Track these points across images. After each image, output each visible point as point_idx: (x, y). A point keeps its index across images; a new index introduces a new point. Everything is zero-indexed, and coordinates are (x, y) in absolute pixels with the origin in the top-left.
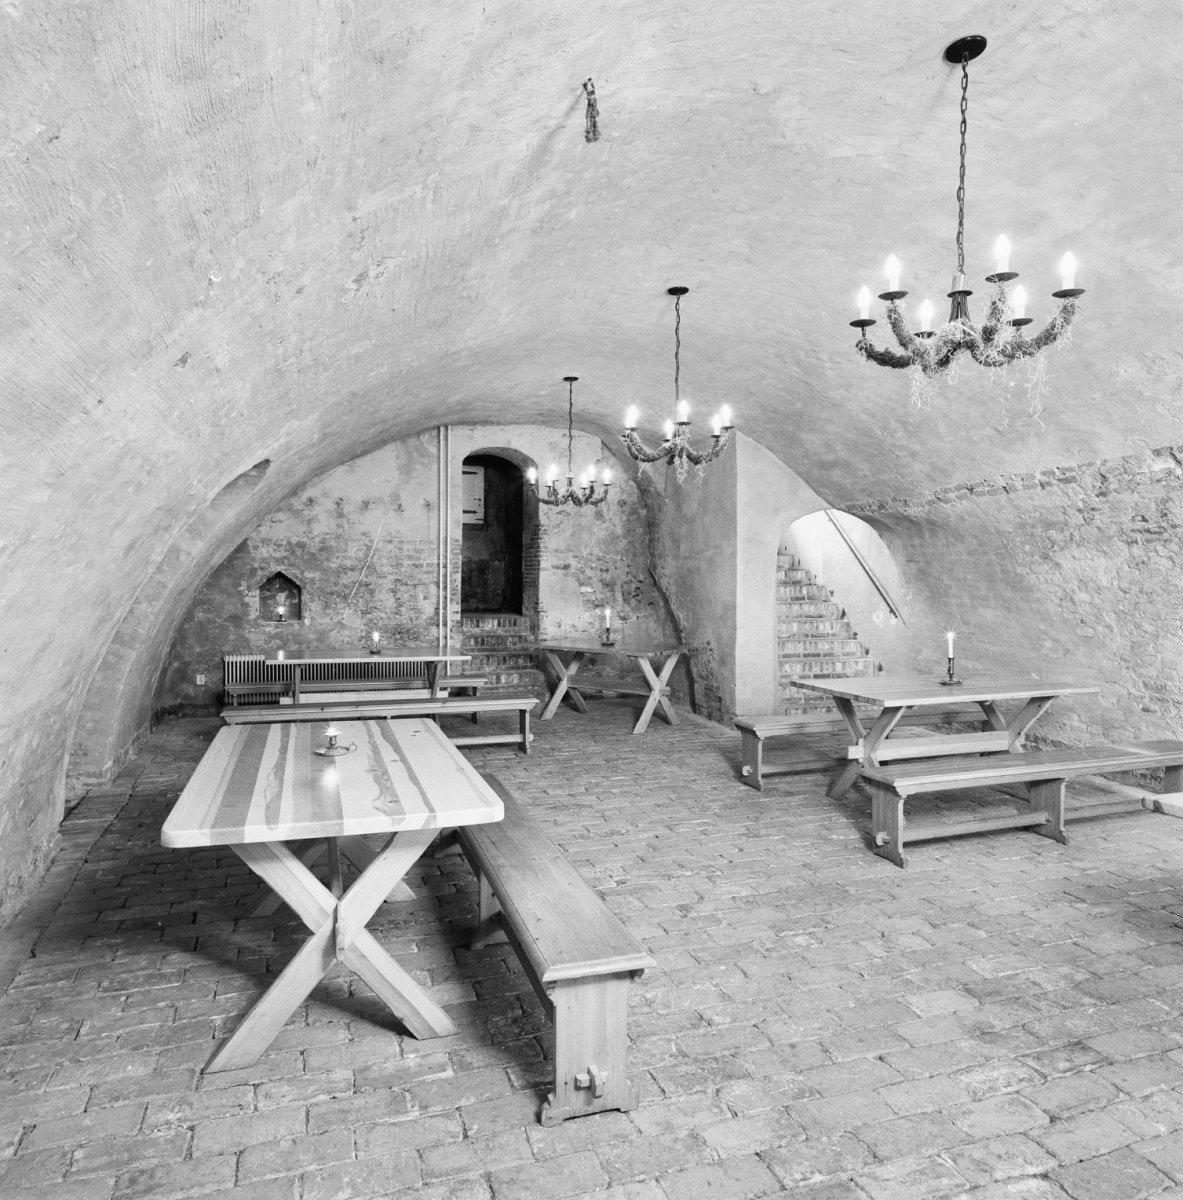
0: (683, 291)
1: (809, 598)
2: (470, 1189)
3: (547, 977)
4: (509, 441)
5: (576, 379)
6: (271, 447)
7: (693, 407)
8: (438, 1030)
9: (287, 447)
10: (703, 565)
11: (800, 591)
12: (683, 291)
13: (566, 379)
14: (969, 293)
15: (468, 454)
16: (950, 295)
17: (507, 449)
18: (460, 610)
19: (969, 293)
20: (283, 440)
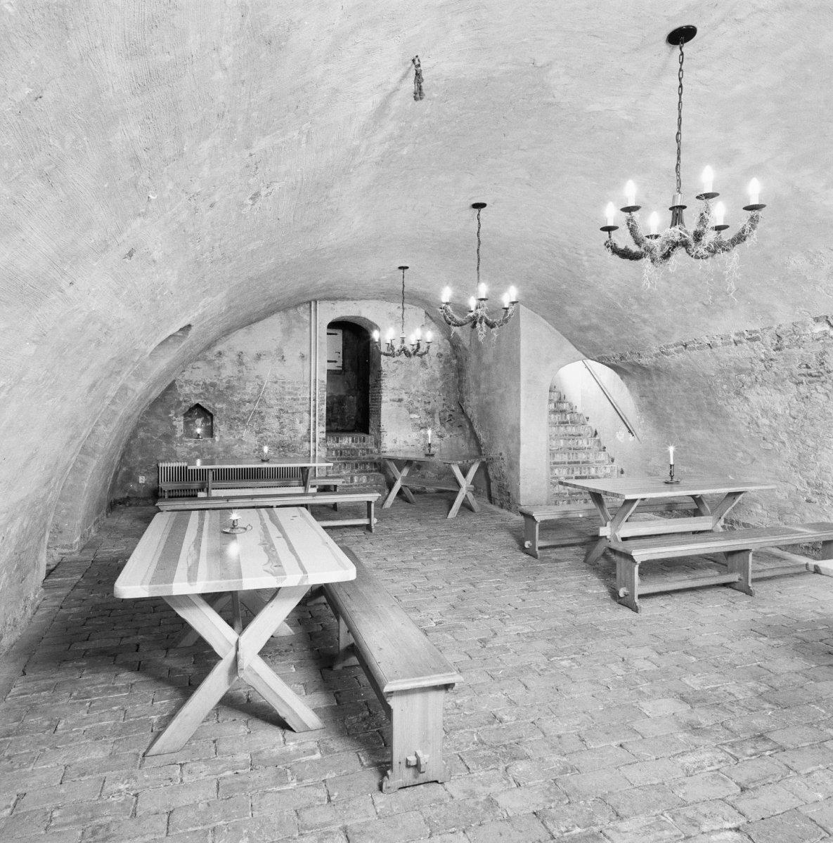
0: (483, 205)
1: (572, 422)
5: (407, 268)
9: (203, 316)
10: (498, 400)
11: (565, 418)
12: (483, 205)
13: (400, 268)
14: (684, 207)
19: (684, 207)
20: (200, 311)
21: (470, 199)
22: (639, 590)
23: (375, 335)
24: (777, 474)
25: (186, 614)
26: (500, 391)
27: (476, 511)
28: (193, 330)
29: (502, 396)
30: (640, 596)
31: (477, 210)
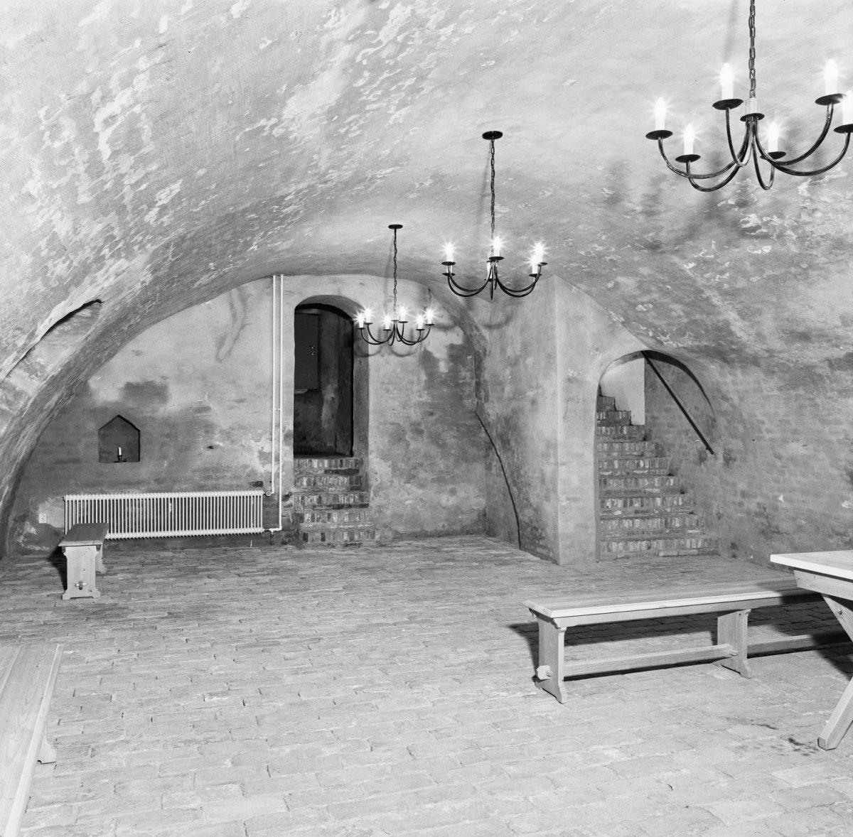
0: (498, 135)
1: (630, 438)
2: (613, 325)
3: (730, 111)
4: (339, 290)
5: (400, 227)
6: (101, 287)
7: (508, 238)
8: (634, 421)
9: (118, 289)
10: (528, 406)
11: (621, 431)
12: (498, 135)
13: (391, 227)
14: (761, 116)
15: (297, 304)
16: (743, 119)
17: (339, 297)
18: (264, 451)
19: (761, 116)
20: (112, 281)
21: (479, 126)
22: (565, 669)
23: (360, 319)
24: (778, 260)
25: (825, 598)
26: (531, 394)
27: (564, 552)
28: (105, 309)
29: (534, 402)
30: (567, 679)
31: (488, 142)
